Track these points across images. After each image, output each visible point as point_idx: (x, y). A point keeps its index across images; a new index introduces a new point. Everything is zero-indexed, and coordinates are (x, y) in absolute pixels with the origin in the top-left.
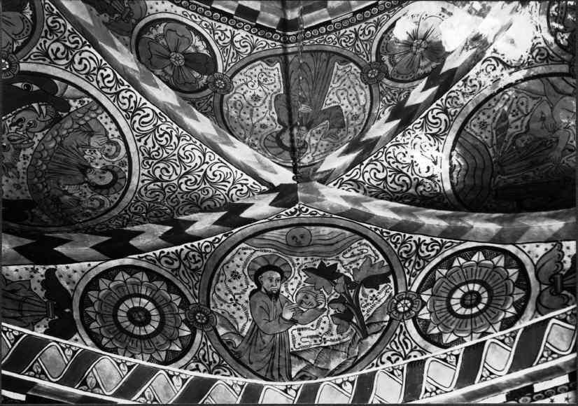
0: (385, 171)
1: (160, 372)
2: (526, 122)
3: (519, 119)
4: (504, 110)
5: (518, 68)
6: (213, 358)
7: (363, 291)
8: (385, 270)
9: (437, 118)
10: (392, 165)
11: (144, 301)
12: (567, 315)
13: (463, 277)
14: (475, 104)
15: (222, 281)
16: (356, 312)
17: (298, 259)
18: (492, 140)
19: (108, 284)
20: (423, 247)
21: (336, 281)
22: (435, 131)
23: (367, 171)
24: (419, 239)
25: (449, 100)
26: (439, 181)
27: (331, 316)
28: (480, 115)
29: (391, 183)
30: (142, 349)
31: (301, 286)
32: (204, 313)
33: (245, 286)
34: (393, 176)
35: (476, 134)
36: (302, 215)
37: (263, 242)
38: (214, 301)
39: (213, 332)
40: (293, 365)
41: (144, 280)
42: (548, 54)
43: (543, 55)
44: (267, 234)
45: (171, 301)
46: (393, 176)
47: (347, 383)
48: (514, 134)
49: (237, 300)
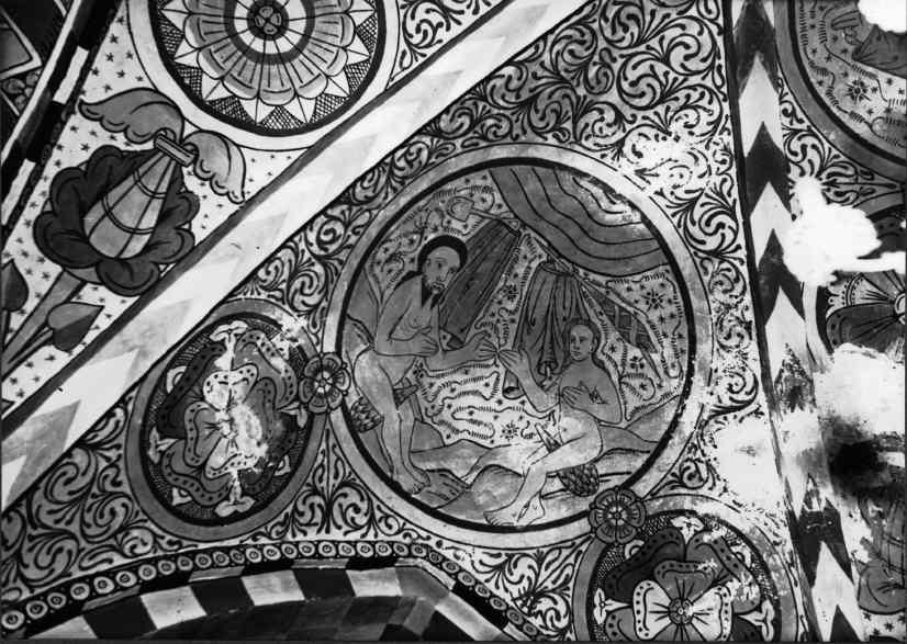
0: (682, 71)
2: (611, 368)
3: (623, 365)
4: (656, 352)
5: (701, 425)
9: (715, 232)
12: (27, 86)
14: (697, 314)
18: (619, 295)
20: (436, 18)
22: (698, 211)
23: (701, 33)
24: (459, 23)
25: (732, 274)
26: (603, 156)
28: (673, 309)
29: (652, 67)
34: (663, 79)
35: (647, 278)
42: (685, 486)
43: (690, 477)
46: (663, 79)
48: (603, 336)
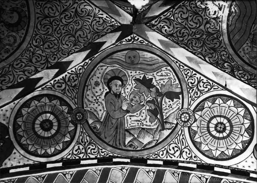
1: (59, 174)
6: (87, 139)
7: (165, 99)
8: (178, 90)
10: (193, 9)
11: (48, 115)
13: (219, 112)
15: (89, 89)
16: (160, 112)
17: (131, 72)
19: (27, 110)
20: (201, 84)
21: (151, 89)
23: (176, 13)
24: (200, 77)
26: (220, 22)
27: (147, 110)
30: (50, 145)
31: (132, 90)
32: (81, 113)
33: (102, 90)
34: (193, 16)
36: (135, 42)
37: (112, 61)
38: (86, 103)
39: (86, 123)
40: (126, 137)
41: (47, 102)
44: (115, 55)
45: (63, 111)
47: (151, 172)
49: (98, 100)
